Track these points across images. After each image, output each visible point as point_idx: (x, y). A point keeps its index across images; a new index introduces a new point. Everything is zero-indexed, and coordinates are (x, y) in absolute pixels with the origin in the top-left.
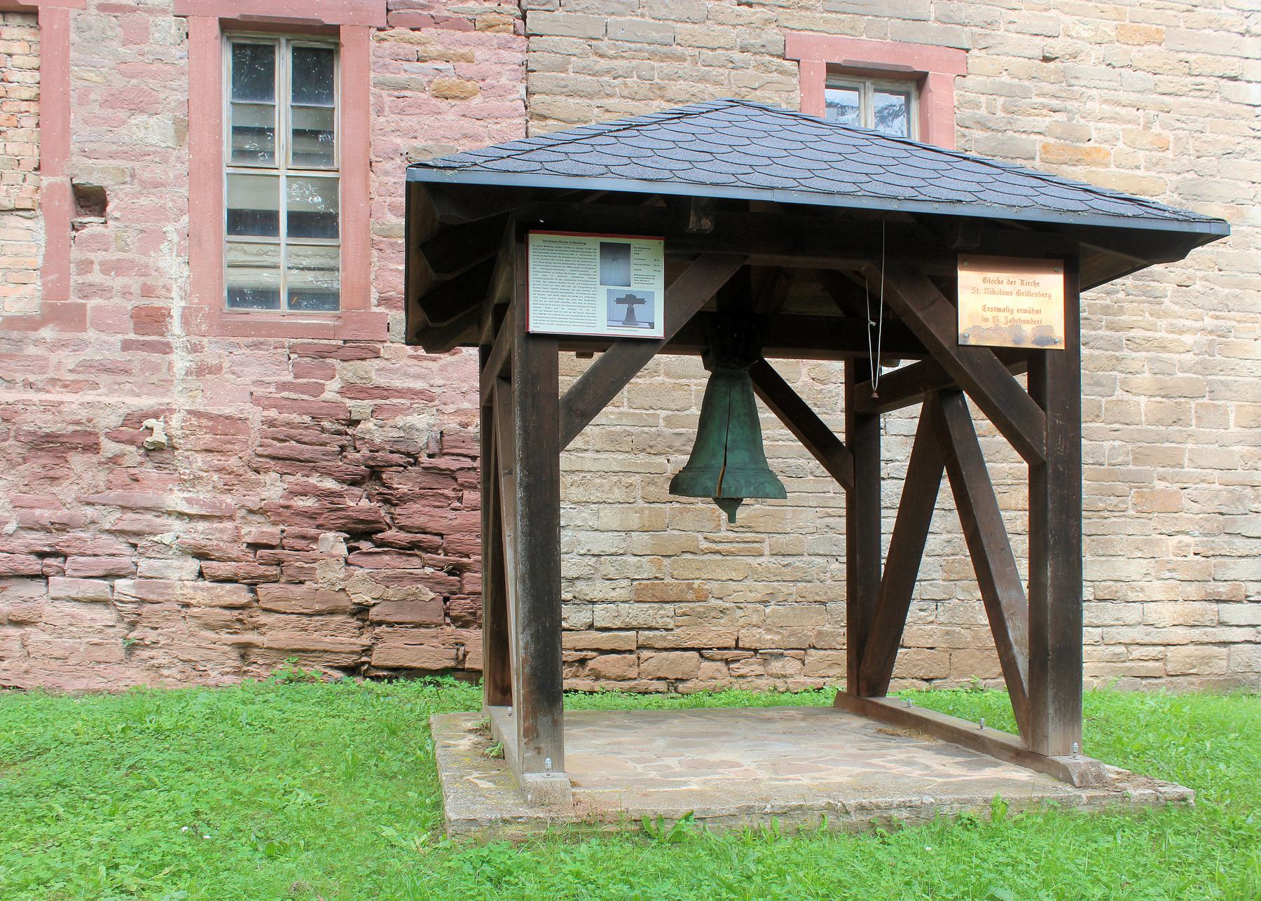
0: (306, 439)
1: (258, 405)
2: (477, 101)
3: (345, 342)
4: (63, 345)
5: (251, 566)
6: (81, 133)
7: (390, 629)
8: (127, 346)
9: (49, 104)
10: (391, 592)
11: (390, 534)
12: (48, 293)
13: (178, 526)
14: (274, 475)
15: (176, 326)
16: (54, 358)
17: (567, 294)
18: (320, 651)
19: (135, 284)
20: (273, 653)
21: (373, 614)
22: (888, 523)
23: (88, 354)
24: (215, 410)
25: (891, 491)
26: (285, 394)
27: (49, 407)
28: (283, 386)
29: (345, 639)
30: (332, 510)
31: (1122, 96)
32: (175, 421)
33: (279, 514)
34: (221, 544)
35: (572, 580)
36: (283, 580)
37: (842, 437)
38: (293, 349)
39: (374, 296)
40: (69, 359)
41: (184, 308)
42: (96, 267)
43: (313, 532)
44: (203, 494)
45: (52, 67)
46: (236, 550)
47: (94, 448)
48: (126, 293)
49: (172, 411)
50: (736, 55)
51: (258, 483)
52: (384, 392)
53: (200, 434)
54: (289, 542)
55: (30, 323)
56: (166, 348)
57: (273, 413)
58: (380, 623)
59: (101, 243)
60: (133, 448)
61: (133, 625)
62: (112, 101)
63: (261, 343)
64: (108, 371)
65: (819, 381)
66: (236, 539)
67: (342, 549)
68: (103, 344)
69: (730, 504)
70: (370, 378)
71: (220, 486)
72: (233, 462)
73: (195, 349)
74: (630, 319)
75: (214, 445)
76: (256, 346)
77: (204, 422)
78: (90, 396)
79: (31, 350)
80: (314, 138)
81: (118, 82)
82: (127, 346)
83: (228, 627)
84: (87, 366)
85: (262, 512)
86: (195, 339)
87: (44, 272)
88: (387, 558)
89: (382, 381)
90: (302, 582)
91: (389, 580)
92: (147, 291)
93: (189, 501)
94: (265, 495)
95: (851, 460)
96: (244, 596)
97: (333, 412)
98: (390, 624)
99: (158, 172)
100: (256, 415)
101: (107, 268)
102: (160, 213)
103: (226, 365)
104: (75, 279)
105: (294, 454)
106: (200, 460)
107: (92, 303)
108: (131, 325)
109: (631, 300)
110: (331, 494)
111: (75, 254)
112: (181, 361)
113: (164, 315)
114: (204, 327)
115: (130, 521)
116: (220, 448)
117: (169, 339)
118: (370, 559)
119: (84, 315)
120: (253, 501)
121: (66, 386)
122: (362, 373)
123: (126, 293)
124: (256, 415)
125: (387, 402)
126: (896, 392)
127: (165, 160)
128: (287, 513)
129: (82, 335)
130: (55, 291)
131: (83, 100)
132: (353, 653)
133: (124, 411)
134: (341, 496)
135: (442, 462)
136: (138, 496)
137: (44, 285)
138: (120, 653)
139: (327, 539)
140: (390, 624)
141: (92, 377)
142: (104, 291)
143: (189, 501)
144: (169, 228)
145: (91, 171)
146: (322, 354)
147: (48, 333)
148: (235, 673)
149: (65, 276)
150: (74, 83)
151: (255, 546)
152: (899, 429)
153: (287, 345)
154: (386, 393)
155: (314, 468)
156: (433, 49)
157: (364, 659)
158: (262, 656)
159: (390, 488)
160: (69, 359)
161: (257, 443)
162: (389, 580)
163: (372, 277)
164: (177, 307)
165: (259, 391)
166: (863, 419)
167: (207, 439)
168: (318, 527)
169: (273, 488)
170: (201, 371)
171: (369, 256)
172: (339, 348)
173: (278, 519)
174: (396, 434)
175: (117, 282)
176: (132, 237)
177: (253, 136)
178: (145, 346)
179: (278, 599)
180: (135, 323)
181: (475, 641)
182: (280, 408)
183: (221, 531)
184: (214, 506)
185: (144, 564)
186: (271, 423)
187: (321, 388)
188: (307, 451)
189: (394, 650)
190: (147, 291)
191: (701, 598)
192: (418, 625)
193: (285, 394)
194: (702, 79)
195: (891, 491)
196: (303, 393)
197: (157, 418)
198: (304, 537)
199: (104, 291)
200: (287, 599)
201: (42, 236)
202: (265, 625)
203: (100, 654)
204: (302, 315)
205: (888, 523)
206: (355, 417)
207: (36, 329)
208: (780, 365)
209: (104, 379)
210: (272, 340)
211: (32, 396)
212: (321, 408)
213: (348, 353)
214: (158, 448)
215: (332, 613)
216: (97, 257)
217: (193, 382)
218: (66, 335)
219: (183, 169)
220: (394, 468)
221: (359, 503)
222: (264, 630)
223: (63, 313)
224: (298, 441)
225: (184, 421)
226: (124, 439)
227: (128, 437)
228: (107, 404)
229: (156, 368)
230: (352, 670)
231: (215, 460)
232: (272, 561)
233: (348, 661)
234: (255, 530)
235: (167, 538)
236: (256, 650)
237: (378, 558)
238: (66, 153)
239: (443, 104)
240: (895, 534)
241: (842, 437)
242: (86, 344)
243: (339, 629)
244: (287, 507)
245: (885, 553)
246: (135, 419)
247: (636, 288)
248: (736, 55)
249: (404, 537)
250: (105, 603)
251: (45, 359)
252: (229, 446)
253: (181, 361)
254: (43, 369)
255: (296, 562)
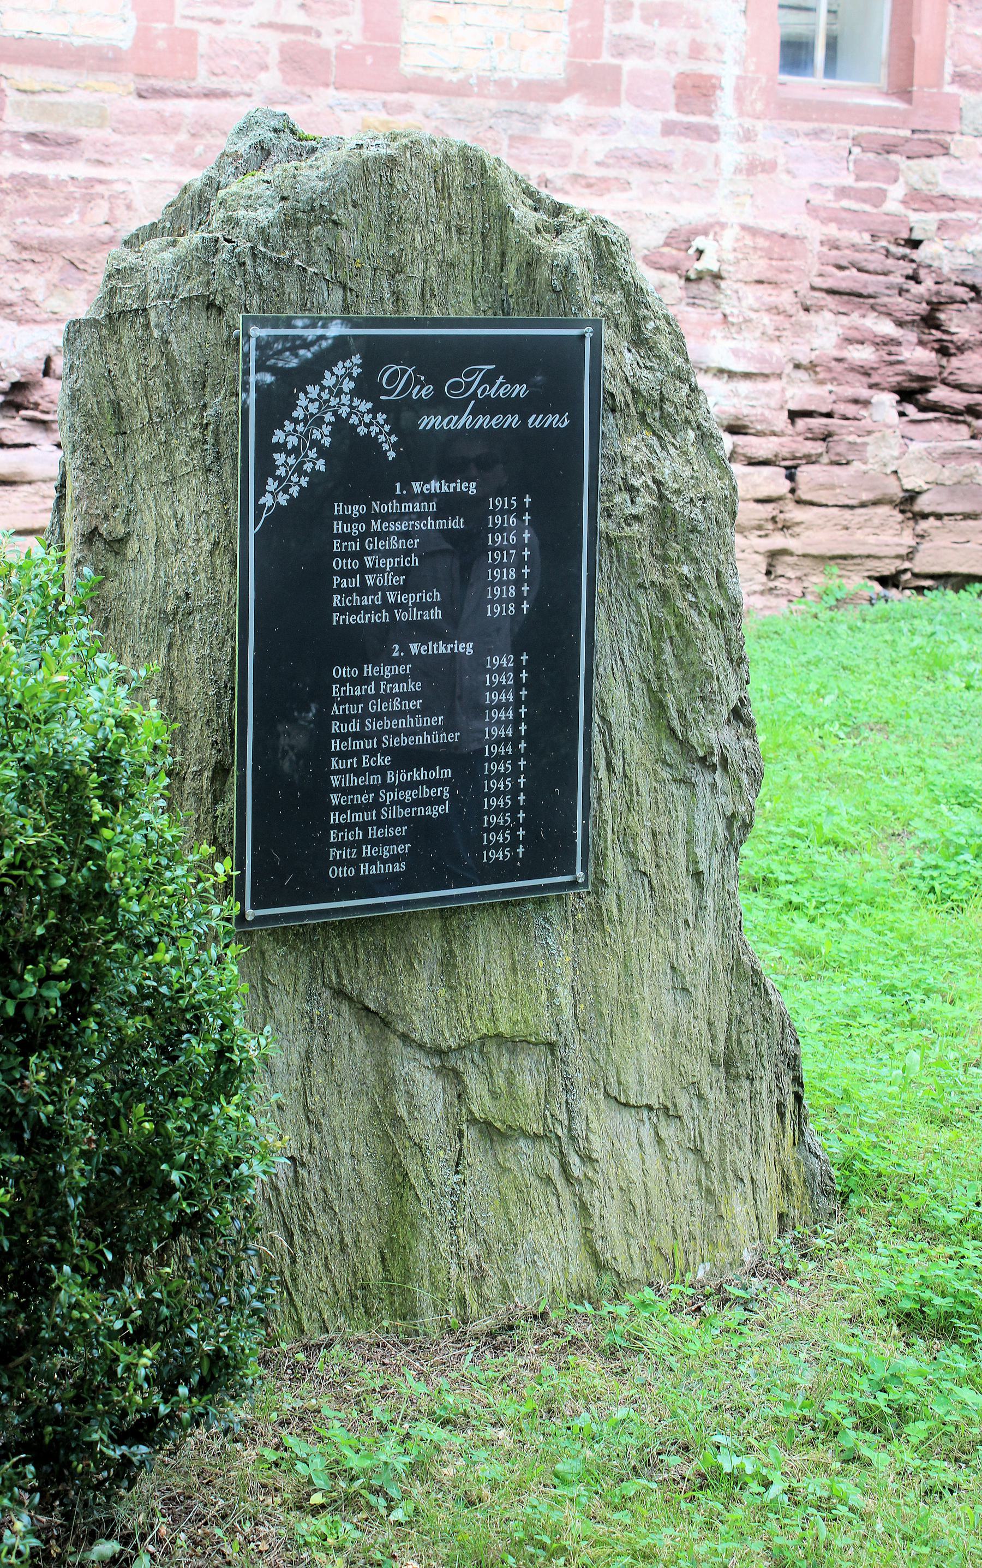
0: (871, 267)
1: (817, 217)
3: (913, 131)
5: (791, 442)
7: (938, 523)
8: (669, 129)
10: (946, 472)
11: (939, 394)
14: (828, 316)
15: (726, 101)
18: (860, 556)
19: (681, 38)
20: (807, 562)
21: (922, 504)
23: (623, 140)
24: (766, 224)
26: (845, 203)
28: (843, 192)
29: (886, 537)
30: (891, 364)
33: (830, 370)
34: (767, 413)
35: (46, 510)
36: (825, 459)
38: (856, 141)
39: (948, 70)
41: (739, 78)
42: (636, 13)
43: (864, 393)
44: (750, 343)
49: (723, 226)
51: (809, 327)
52: (950, 201)
53: (754, 258)
54: (841, 408)
55: (553, 92)
57: (832, 230)
58: (925, 516)
60: (673, 278)
63: (823, 131)
64: (644, 165)
70: (936, 184)
71: (770, 331)
72: (785, 298)
73: (748, 136)
75: (768, 275)
76: (816, 134)
77: (762, 242)
82: (669, 129)
83: (759, 528)
84: (619, 157)
85: (812, 367)
86: (748, 122)
87: (573, 16)
88: (936, 426)
89: (949, 188)
90: (848, 463)
92: (696, 51)
93: (736, 353)
94: (816, 343)
97: (895, 229)
98: (939, 517)
100: (815, 231)
103: (781, 161)
104: (610, 28)
105: (858, 288)
106: (752, 295)
107: (630, 64)
108: (672, 98)
113: (714, 87)
114: (759, 106)
116: (775, 279)
117: (716, 120)
118: (920, 428)
119: (619, 82)
121: (589, 186)
122: (929, 177)
123: (671, 53)
124: (815, 231)
125: (953, 215)
128: (838, 367)
129: (614, 112)
130: (585, 45)
132: (898, 557)
133: (668, 225)
134: (899, 344)
137: (573, 35)
139: (881, 403)
140: (939, 517)
141: (623, 174)
142: (643, 48)
143: (736, 353)
146: (889, 149)
147: (573, 106)
148: (762, 593)
151: (794, 415)
153: (851, 134)
154: (951, 204)
155: (873, 308)
157: (907, 565)
158: (793, 566)
159: (946, 332)
160: (596, 146)
161: (814, 272)
163: (948, 43)
165: (818, 199)
167: (760, 267)
168: (871, 387)
170: (754, 168)
171: (944, 15)
172: (907, 140)
173: (828, 376)
174: (964, 260)
179: (822, 486)
180: (679, 97)
182: (840, 222)
183: (769, 395)
184: (763, 360)
187: (879, 197)
188: (871, 283)
190: (696, 51)
192: (967, 516)
193: (845, 203)
196: (864, 201)
197: (706, 234)
198: (856, 401)
199: (643, 48)
200: (832, 487)
202: (798, 524)
204: (855, 89)
206: (916, 236)
207: (558, 100)
209: (637, 176)
210: (835, 127)
212: (884, 223)
213: (917, 148)
215: (875, 503)
218: (596, 111)
220: (956, 306)
221: (918, 358)
222: (797, 529)
224: (859, 270)
225: (737, 240)
226: (666, 265)
227: (673, 263)
233: (887, 568)
234: (802, 392)
236: (788, 559)
237: (926, 426)
242: (617, 124)
244: (839, 360)
246: (681, 238)
249: (958, 399)
251: (569, 145)
252: (785, 276)
253: (730, 152)
254: (564, 160)
255: (846, 433)
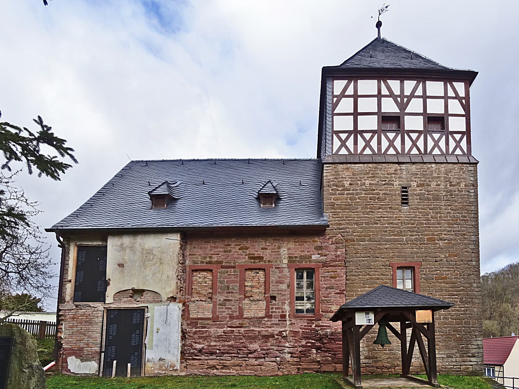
2: (338, 278)
4: (268, 321)
6: (272, 288)
9: (266, 283)
12: (266, 313)
13: (287, 349)
15: (287, 317)
16: (267, 323)
17: (361, 320)
19: (281, 311)
22: (408, 345)
25: (408, 339)
27: (266, 331)
28: (305, 326)
31: (450, 266)
32: (287, 332)
37: (400, 332)
40: (269, 323)
45: (267, 277)
46: (297, 353)
47: (274, 337)
48: (279, 312)
50: (381, 267)
55: (263, 318)
56: (286, 321)
59: (275, 304)
61: (279, 365)
62: (277, 282)
65: (397, 325)
66: (297, 351)
67: (315, 352)
68: (275, 321)
69: (383, 345)
74: (369, 322)
78: (273, 329)
79: (263, 322)
80: (310, 285)
81: (278, 279)
82: (279, 320)
84: (272, 324)
85: (302, 346)
87: (265, 310)
89: (322, 324)
91: (323, 357)
92: (283, 312)
95: (402, 336)
96: (299, 360)
99: (285, 293)
101: (276, 308)
102: (285, 299)
104: (271, 310)
109: (369, 320)
110: (313, 343)
111: (271, 307)
112: (288, 323)
115: (280, 348)
120: (300, 344)
126: (409, 326)
127: (286, 291)
131: (272, 282)
135: (332, 337)
136: (281, 344)
138: (277, 369)
142: (275, 312)
144: (286, 302)
145: (273, 293)
147: (266, 319)
149: (269, 310)
150: (271, 280)
152: (409, 331)
156: (330, 270)
160: (269, 323)
162: (323, 357)
164: (288, 314)
166: (403, 329)
169: (304, 342)
170: (291, 324)
175: (278, 311)
176: (280, 304)
177: (300, 287)
178: (282, 320)
181: (340, 367)
185: (281, 355)
186: (303, 332)
189: (325, 368)
190: (283, 312)
191: (376, 358)
194: (376, 272)
195: (408, 339)
199: (275, 312)
201: (265, 304)
203: (274, 370)
205: (408, 345)
208: (391, 323)
209: (275, 326)
211: (263, 329)
214: (284, 336)
216: (274, 307)
217: (290, 326)
219: (289, 292)
223: (268, 316)
228: (276, 330)
229: (284, 324)
230: (317, 372)
231: (294, 338)
232: (304, 354)
235: (286, 351)
238: (269, 291)
239: (332, 279)
240: (410, 342)
241: (400, 332)
243: (315, 365)
245: (408, 347)
247: (370, 318)
248: (381, 267)
250: (275, 362)
253: (288, 323)
